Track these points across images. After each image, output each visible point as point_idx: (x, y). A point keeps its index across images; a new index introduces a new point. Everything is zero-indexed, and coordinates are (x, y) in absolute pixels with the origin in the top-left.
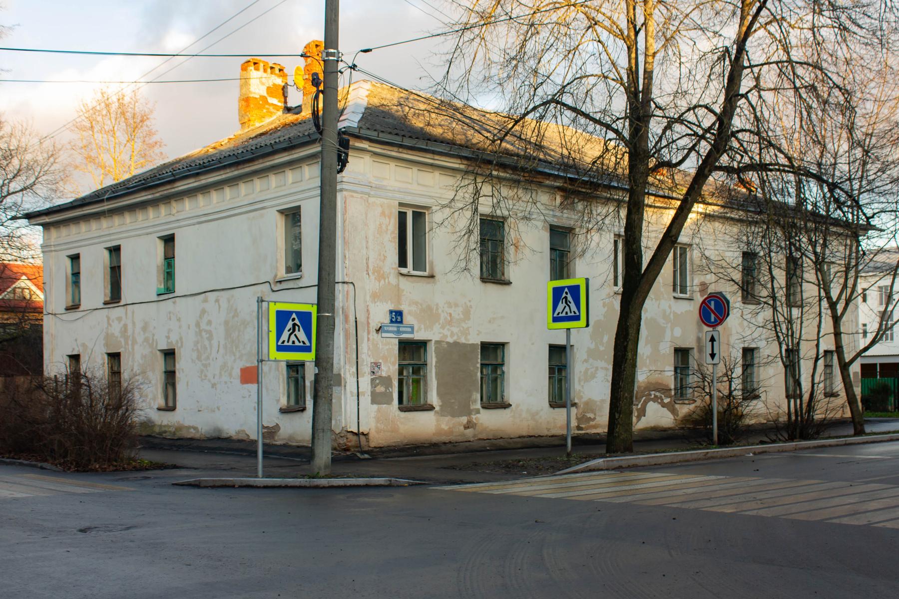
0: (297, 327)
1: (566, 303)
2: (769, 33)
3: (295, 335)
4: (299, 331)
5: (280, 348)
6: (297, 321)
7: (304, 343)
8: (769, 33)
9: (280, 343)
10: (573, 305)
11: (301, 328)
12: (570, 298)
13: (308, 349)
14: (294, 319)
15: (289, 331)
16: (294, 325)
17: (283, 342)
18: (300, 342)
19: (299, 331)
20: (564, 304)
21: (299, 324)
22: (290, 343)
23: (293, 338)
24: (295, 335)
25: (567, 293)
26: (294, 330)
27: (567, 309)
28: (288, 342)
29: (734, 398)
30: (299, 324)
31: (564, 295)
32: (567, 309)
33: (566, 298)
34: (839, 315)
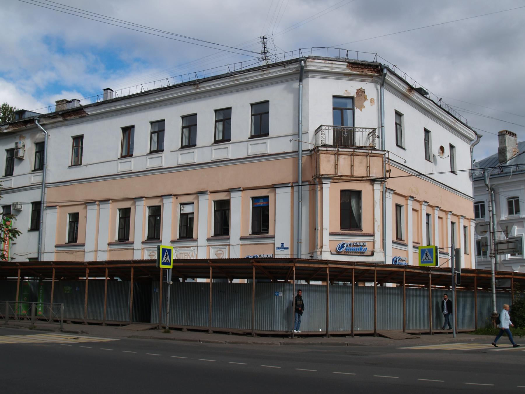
1: (427, 255)
5: (163, 263)
6: (167, 254)
7: (430, 260)
13: (169, 264)
14: (166, 253)
16: (167, 255)
17: (424, 260)
18: (428, 259)
21: (168, 255)
27: (427, 258)
30: (168, 255)
32: (427, 258)
33: (426, 254)
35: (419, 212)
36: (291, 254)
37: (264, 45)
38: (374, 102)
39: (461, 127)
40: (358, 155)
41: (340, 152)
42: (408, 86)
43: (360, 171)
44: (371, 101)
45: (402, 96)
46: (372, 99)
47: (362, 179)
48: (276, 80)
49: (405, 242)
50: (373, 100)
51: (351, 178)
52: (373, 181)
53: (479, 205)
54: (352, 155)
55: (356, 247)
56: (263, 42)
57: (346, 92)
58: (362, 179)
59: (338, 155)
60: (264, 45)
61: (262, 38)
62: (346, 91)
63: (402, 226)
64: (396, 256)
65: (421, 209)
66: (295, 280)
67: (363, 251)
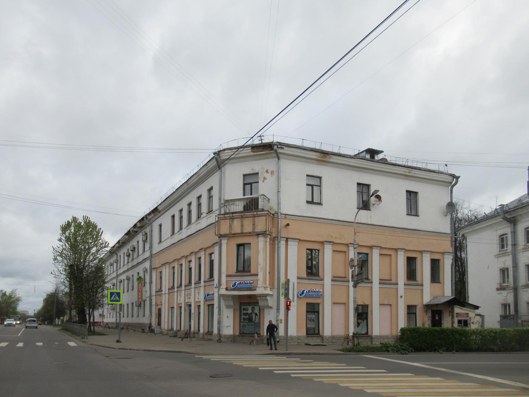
5: (111, 301)
6: (116, 295)
16: (115, 296)
23: (115, 298)
35: (347, 253)
36: (514, 289)
37: (261, 141)
38: (274, 173)
39: (422, 173)
40: (247, 217)
41: (234, 217)
42: (320, 153)
43: (248, 228)
44: (271, 174)
45: (317, 162)
46: (272, 171)
47: (249, 234)
48: (311, 161)
49: (321, 277)
50: (273, 172)
51: (242, 234)
52: (258, 235)
53: (504, 237)
54: (242, 217)
55: (244, 285)
56: (261, 139)
57: (252, 170)
58: (249, 234)
59: (233, 219)
60: (261, 141)
61: (259, 136)
62: (253, 169)
63: (319, 265)
64: (2, 289)
65: (349, 250)
67: (251, 286)
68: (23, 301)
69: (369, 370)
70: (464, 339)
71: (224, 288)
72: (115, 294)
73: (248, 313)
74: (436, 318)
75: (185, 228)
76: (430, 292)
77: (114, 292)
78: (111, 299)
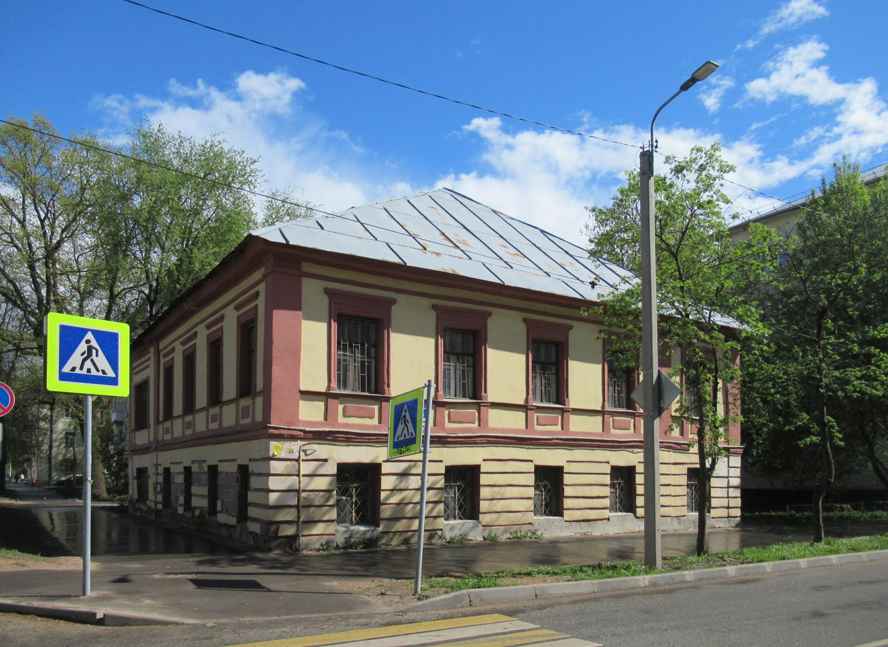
0: (94, 351)
2: (24, 213)
3: (92, 361)
4: (97, 356)
5: (63, 377)
6: (94, 343)
7: (104, 372)
8: (24, 213)
9: (63, 370)
10: (410, 425)
11: (100, 352)
12: (408, 418)
13: (114, 381)
15: (82, 355)
16: (90, 349)
17: (74, 369)
18: (98, 370)
19: (97, 356)
20: (403, 425)
22: (84, 372)
23: (88, 364)
24: (92, 361)
25: (406, 411)
26: (90, 354)
28: (81, 368)
29: (525, 537)
31: (404, 413)
32: (405, 432)
33: (405, 416)
34: (285, 242)
66: (689, 469)
68: (852, 111)
69: (247, 306)
70: (459, 54)
71: (714, 508)
72: (88, 342)
73: (94, 614)
74: (642, 305)
75: (441, 461)
76: (115, 397)
77: (83, 331)
78: (67, 369)
